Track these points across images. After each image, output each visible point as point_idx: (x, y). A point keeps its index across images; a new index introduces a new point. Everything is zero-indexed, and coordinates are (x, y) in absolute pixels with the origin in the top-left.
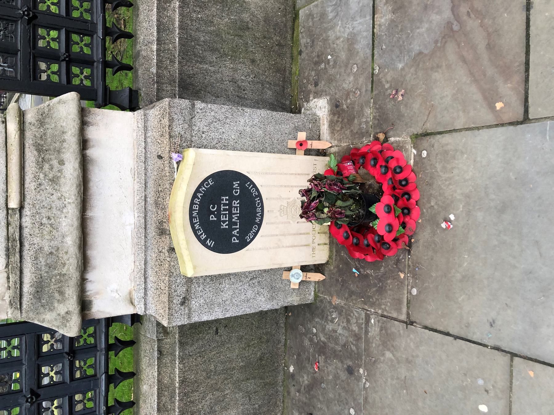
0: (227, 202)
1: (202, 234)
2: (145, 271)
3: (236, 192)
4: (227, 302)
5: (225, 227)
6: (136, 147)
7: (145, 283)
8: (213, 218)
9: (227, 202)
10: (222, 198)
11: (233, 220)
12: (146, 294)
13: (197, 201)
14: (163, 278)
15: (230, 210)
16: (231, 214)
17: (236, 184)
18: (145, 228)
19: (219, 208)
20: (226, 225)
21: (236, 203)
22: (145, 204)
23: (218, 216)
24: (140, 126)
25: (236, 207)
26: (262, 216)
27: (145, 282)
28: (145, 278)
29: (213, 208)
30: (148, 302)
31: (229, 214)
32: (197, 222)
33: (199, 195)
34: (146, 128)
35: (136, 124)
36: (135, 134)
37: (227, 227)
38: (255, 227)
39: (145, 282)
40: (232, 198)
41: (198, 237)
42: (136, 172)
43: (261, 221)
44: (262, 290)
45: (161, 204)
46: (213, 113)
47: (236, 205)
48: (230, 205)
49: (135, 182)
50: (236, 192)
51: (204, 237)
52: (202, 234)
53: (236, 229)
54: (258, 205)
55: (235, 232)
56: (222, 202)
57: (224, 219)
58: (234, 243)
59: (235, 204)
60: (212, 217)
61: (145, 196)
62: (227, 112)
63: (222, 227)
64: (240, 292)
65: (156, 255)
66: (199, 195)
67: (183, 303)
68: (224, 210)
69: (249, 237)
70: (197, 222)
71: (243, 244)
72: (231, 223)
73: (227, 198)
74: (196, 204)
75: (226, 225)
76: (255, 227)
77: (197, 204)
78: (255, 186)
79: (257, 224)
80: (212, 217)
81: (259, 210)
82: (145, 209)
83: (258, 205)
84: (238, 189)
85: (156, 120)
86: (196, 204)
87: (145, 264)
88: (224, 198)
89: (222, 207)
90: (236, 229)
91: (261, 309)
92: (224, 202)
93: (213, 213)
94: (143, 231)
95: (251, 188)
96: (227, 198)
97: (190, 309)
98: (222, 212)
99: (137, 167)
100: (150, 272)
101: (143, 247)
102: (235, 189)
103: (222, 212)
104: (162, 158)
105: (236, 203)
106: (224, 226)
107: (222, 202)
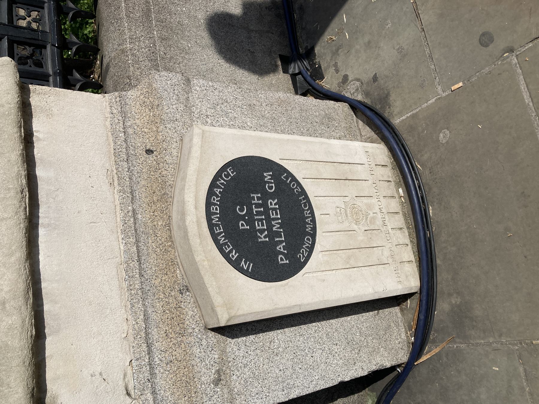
0: (260, 202)
1: (231, 251)
2: (147, 334)
3: (271, 188)
4: (288, 373)
5: (264, 240)
6: (111, 139)
7: (149, 354)
8: (243, 226)
9: (260, 202)
10: (237, 254)
11: (274, 229)
12: (152, 374)
13: (215, 200)
14: (179, 339)
15: (266, 212)
16: (269, 220)
17: (267, 176)
18: (139, 261)
19: (250, 210)
20: (265, 237)
21: (272, 203)
22: (135, 224)
23: (251, 222)
24: (115, 111)
25: (275, 209)
26: (314, 221)
27: (150, 352)
28: (149, 346)
29: (242, 210)
30: (158, 388)
31: (267, 221)
32: (221, 233)
33: (218, 191)
34: (124, 114)
35: (109, 110)
36: (108, 123)
37: (267, 239)
38: (308, 239)
39: (150, 352)
40: (266, 196)
41: (226, 256)
42: (116, 176)
43: (314, 229)
44: (335, 347)
45: (163, 196)
46: (216, 93)
47: (273, 206)
48: (264, 205)
49: (115, 191)
50: (271, 188)
51: (234, 255)
52: (231, 251)
53: (281, 242)
54: (305, 206)
55: (280, 248)
56: (253, 202)
57: (261, 227)
58: (282, 264)
59: (271, 204)
60: (242, 225)
61: (134, 210)
62: (235, 93)
63: (260, 240)
64: (303, 353)
65: (162, 303)
66: (218, 191)
67: (217, 382)
68: (258, 213)
69: (303, 254)
70: (221, 233)
71: (295, 267)
72: (272, 234)
73: (259, 195)
74: (215, 204)
75: (265, 237)
76: (308, 239)
77: (217, 205)
78: (294, 179)
79: (309, 234)
80: (242, 225)
81: (307, 213)
82: (136, 230)
83: (305, 206)
84: (272, 183)
85: (138, 103)
86: (215, 204)
87: (146, 319)
88: (255, 196)
89: (255, 210)
90: (281, 242)
91: (340, 379)
92: (256, 201)
93: (242, 218)
94: (137, 264)
95: (290, 182)
96: (259, 195)
97: (231, 391)
98: (256, 217)
99: (117, 169)
100: (154, 333)
101: (139, 292)
102: (269, 183)
103: (256, 217)
104: (152, 152)
105: (272, 203)
106: (263, 238)
107: (253, 202)
